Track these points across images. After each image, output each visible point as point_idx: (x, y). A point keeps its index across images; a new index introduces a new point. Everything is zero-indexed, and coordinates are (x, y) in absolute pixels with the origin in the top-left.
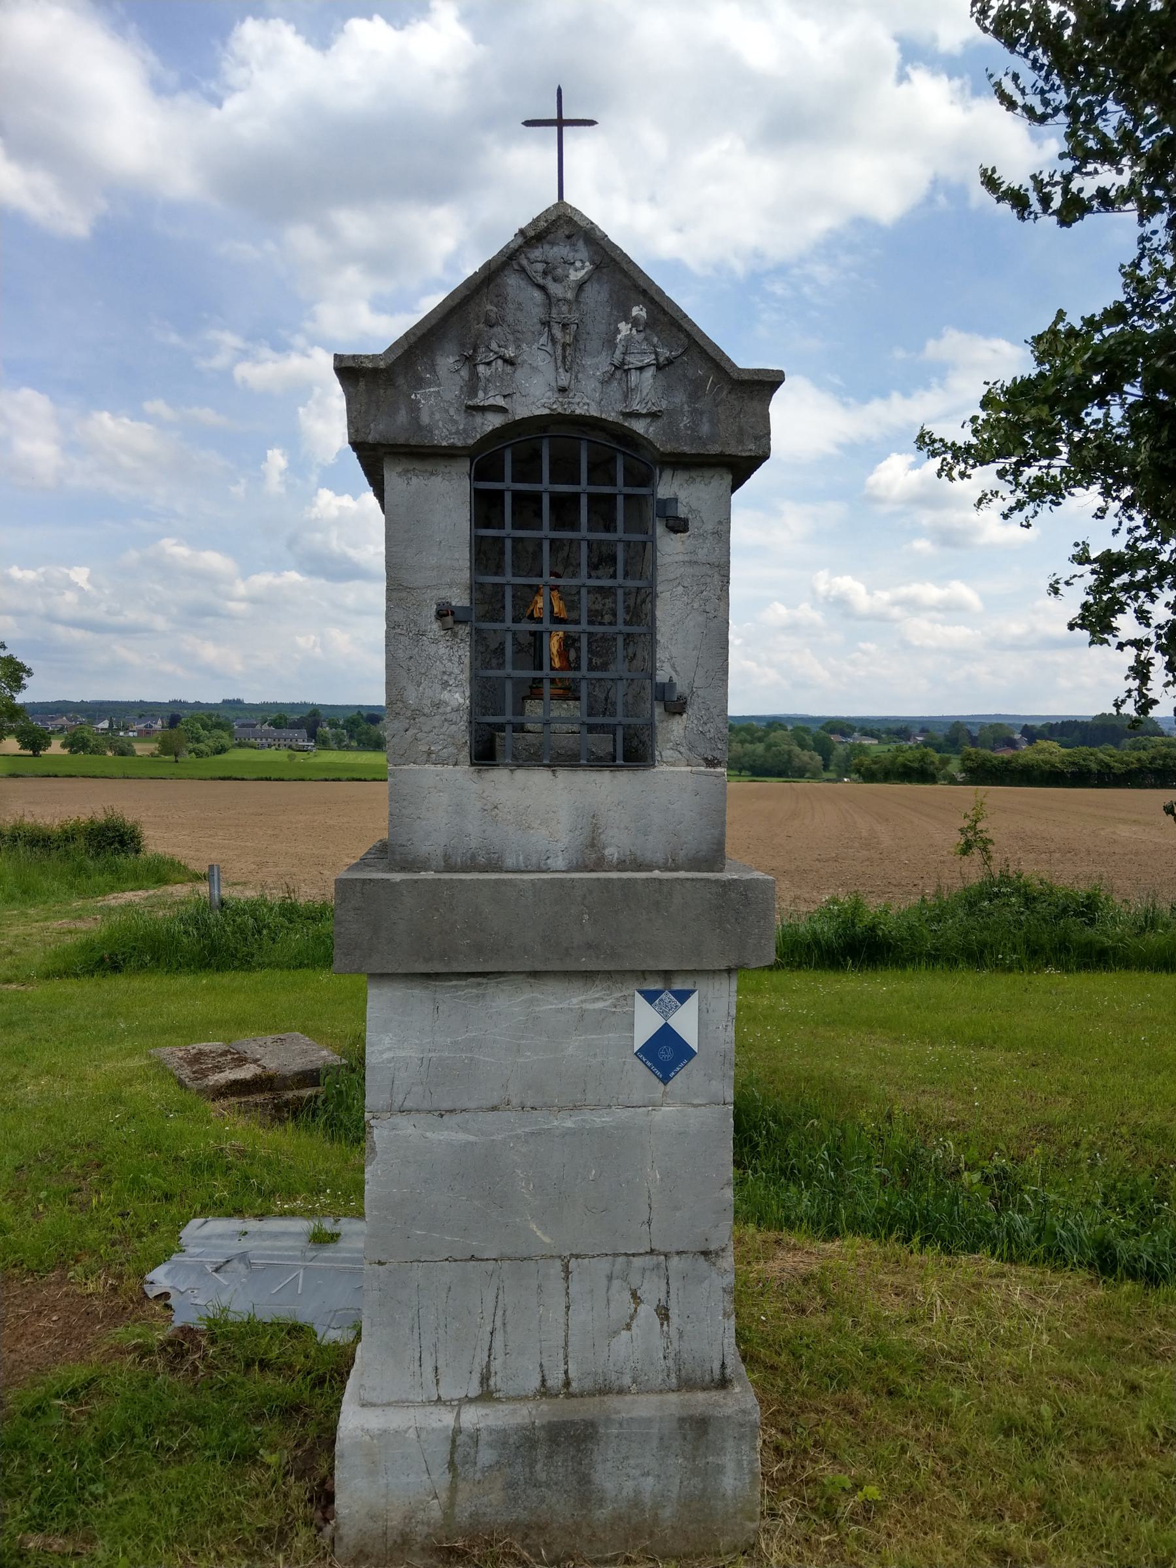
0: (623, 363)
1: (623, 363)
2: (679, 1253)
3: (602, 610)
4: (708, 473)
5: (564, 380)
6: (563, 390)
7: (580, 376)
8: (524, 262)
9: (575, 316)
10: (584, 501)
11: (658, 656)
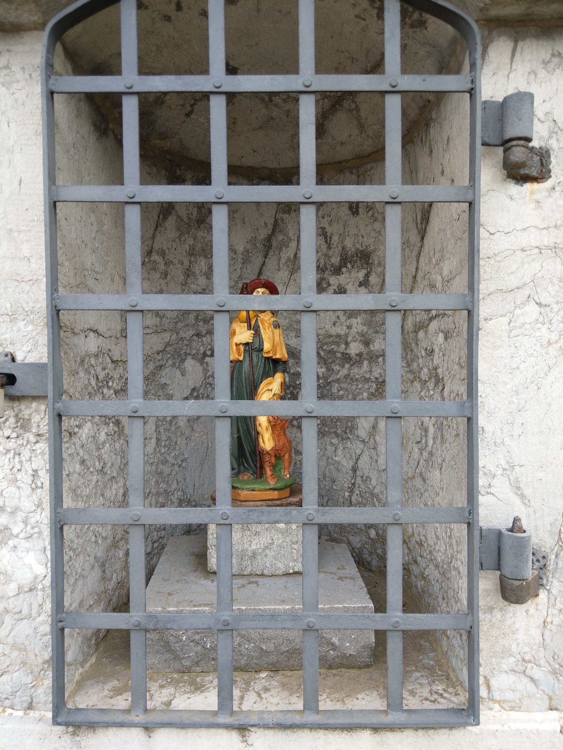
3: (347, 335)
11: (481, 464)
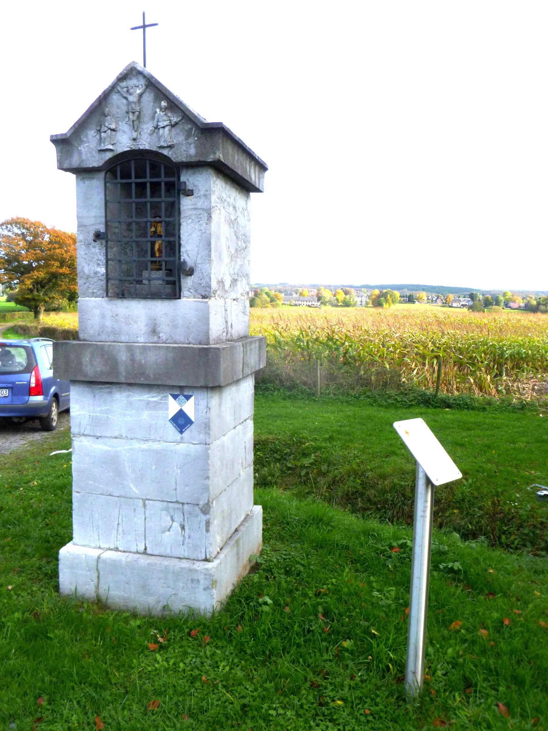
0: (157, 126)
1: (157, 126)
2: (187, 504)
4: (201, 169)
5: (135, 135)
6: (134, 140)
7: (142, 133)
8: (119, 88)
9: (138, 108)
10: (148, 185)
